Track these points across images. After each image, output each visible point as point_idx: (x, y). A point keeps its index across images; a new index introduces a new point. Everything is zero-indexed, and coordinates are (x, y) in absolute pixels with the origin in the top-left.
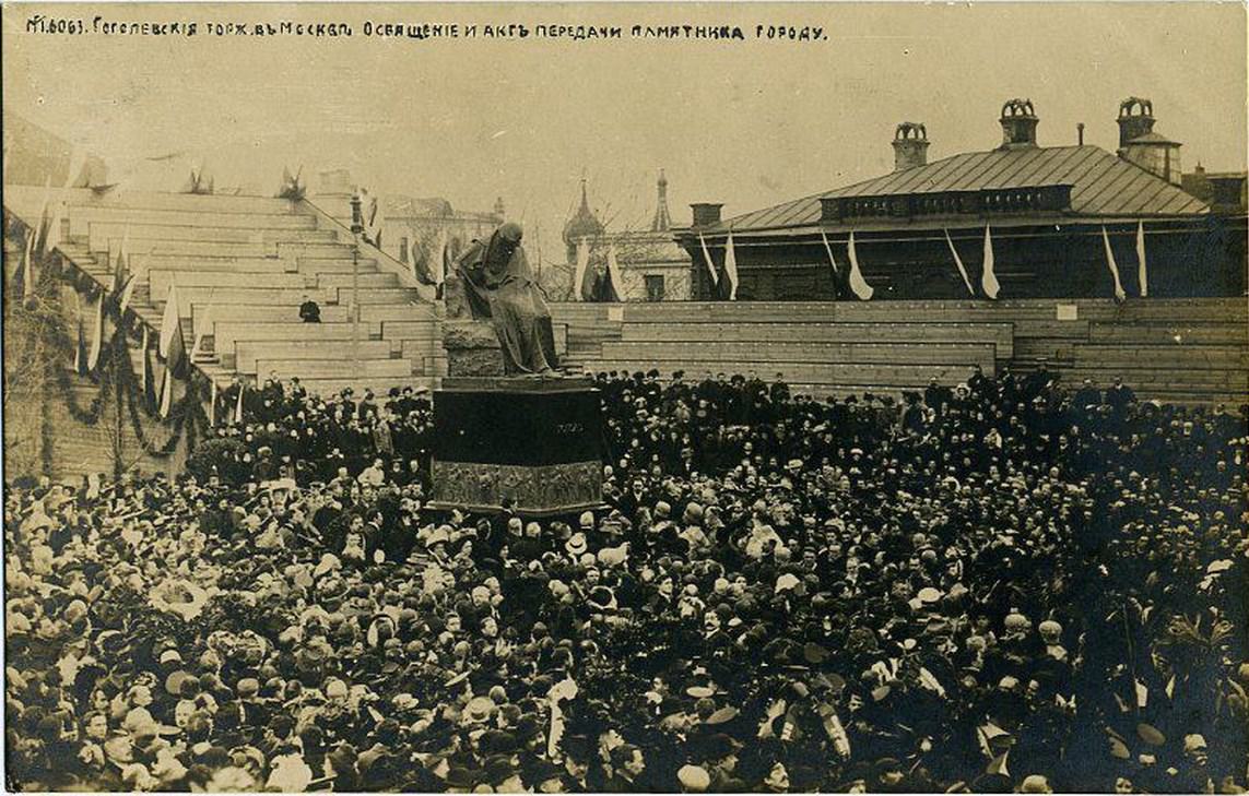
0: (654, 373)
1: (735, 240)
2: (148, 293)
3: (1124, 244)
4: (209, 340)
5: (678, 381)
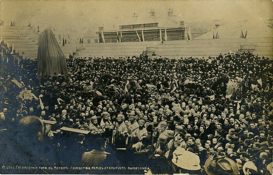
0: (182, 58)
1: (103, 33)
2: (3, 43)
3: (163, 32)
4: (14, 51)
5: (182, 59)
